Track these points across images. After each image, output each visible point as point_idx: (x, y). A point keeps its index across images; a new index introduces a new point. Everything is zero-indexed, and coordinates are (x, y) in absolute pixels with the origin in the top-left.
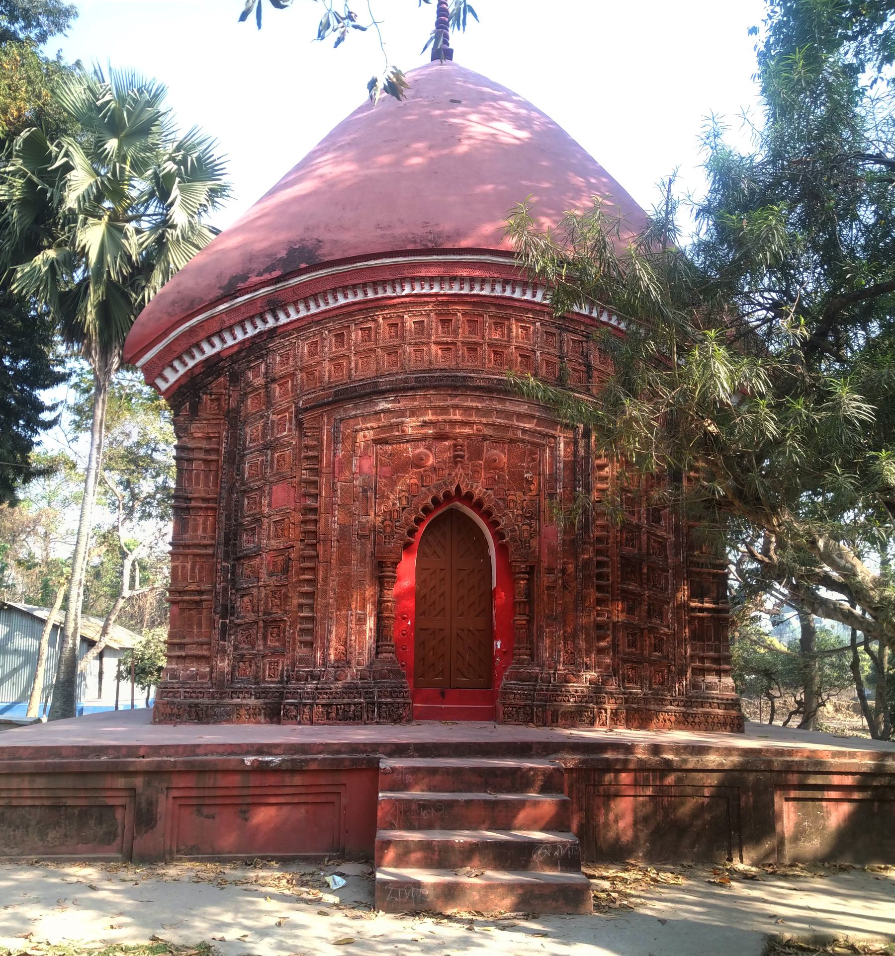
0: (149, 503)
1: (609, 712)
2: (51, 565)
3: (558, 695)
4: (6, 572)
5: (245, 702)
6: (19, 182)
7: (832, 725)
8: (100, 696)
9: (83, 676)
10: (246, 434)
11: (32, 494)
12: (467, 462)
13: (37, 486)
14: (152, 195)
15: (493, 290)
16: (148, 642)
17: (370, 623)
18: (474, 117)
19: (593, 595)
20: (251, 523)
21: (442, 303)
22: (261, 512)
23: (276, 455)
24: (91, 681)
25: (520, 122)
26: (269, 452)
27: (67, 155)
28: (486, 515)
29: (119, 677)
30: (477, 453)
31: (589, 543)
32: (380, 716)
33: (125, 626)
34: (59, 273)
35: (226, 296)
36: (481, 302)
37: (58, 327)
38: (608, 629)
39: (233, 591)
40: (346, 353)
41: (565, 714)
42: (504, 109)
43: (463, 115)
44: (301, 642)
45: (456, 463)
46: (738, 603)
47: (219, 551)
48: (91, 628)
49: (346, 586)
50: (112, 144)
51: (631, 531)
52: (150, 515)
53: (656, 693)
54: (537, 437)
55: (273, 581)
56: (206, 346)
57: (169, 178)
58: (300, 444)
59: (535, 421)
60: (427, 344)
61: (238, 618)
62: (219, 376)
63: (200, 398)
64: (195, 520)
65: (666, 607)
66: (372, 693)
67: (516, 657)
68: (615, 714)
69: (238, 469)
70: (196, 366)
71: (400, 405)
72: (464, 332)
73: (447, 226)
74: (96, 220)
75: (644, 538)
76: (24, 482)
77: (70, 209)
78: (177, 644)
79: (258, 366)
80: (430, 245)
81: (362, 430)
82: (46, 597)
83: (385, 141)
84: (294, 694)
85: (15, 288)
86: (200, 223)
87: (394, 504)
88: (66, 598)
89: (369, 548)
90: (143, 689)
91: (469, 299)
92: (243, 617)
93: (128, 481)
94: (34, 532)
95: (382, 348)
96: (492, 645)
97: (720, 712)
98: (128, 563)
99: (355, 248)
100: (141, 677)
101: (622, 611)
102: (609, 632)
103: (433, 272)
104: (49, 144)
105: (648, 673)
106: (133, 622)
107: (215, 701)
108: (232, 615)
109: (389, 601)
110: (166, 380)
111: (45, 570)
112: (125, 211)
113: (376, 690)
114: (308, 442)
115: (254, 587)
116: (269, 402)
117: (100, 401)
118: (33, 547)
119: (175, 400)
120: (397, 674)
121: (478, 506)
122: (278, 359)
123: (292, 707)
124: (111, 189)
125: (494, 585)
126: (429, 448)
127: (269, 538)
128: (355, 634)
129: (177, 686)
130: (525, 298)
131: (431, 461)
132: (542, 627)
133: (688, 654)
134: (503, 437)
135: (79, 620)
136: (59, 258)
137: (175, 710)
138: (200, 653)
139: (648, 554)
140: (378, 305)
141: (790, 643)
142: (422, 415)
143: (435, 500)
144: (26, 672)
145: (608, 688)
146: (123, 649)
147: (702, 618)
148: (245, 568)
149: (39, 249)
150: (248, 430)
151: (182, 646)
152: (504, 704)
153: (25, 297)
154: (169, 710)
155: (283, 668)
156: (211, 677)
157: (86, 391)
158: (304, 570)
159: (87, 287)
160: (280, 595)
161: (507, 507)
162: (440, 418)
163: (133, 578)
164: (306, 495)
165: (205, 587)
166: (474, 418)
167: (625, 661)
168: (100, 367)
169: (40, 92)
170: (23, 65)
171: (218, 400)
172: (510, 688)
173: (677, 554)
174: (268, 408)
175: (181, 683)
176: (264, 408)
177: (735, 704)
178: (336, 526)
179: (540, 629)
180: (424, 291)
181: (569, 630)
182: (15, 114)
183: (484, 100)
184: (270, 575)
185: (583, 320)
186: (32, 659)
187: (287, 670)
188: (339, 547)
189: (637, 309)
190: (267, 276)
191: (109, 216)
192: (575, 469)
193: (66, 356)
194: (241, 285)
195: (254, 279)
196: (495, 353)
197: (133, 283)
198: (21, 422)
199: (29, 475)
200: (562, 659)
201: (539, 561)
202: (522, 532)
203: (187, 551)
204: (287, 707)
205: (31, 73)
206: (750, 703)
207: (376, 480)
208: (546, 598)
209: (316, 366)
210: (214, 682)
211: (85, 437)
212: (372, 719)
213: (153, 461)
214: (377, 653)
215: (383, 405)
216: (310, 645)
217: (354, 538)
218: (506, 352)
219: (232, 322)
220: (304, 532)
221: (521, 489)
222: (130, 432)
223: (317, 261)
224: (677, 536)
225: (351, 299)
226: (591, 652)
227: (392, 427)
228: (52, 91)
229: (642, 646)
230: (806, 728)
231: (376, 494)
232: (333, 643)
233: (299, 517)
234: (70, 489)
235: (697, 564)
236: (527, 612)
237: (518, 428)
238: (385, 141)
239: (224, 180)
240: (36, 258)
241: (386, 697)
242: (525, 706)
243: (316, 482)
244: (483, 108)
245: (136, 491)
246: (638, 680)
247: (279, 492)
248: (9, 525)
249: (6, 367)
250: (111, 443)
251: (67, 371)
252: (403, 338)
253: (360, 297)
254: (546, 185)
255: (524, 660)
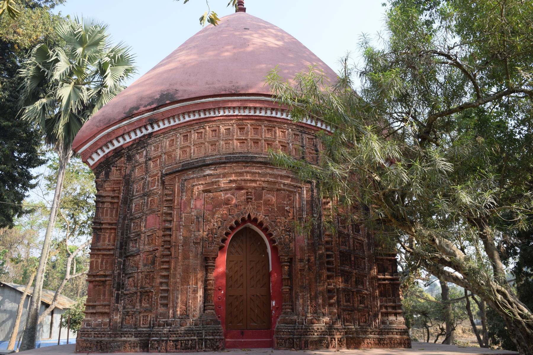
0: (84, 226)
1: (336, 340)
2: (30, 261)
3: (308, 332)
4: (4, 265)
5: (128, 339)
6: (32, 68)
7: (461, 341)
8: (50, 337)
9: (41, 324)
10: (134, 188)
11: (21, 222)
12: (254, 201)
13: (25, 219)
14: (97, 72)
15: (266, 113)
16: (79, 305)
17: (200, 293)
18: (255, 35)
19: (325, 273)
20: (136, 236)
21: (240, 119)
22: (140, 231)
23: (150, 199)
24: (46, 328)
25: (276, 37)
26: (146, 198)
27: (57, 55)
28: (265, 230)
29: (61, 325)
30: (259, 197)
31: (322, 245)
32: (206, 347)
33: (68, 296)
34: (47, 110)
35: (127, 117)
36: (260, 119)
37: (43, 137)
38: (334, 292)
39: (124, 275)
40: (189, 145)
41: (312, 342)
42: (270, 32)
43: (250, 34)
44: (161, 304)
45: (248, 202)
46: (406, 275)
47: (117, 252)
48: (48, 297)
49: (186, 271)
50: (80, 50)
51: (344, 238)
52: (84, 233)
53: (362, 327)
54: (291, 188)
55: (146, 269)
56: (115, 142)
57: (106, 64)
58: (163, 193)
59: (290, 179)
60: (232, 140)
61: (126, 290)
62: (121, 158)
63: (110, 169)
64: (104, 235)
65: (365, 278)
66: (201, 333)
67: (284, 310)
68: (340, 341)
69: (129, 207)
70: (109, 152)
71: (218, 172)
72: (251, 134)
73: (242, 83)
74: (68, 85)
75: (351, 241)
76: (18, 217)
77: (56, 80)
78: (91, 306)
79: (142, 152)
80: (233, 92)
81: (196, 185)
82: (25, 279)
83: (212, 45)
84: (156, 335)
85: (24, 118)
86: (119, 85)
87: (214, 225)
88: (35, 280)
89: (200, 250)
90: (74, 332)
91: (254, 118)
92: (128, 290)
93: (73, 214)
94: (21, 243)
95: (208, 142)
96: (270, 304)
97: (398, 337)
98: (70, 260)
99: (195, 93)
100: (73, 326)
101: (342, 282)
102: (335, 294)
103: (235, 105)
104: (49, 50)
105: (357, 316)
106: (72, 293)
107: (111, 339)
108: (123, 288)
109: (211, 280)
110: (93, 160)
111: (26, 264)
112: (83, 80)
113: (204, 332)
114: (167, 192)
115: (135, 272)
116: (147, 171)
117: (62, 173)
118: (21, 251)
119: (97, 170)
120: (216, 322)
121: (260, 225)
122: (153, 148)
123: (156, 342)
124: (76, 70)
125: (271, 269)
126: (233, 194)
127: (144, 245)
128: (192, 300)
129: (90, 330)
130: (283, 117)
131: (234, 201)
132: (298, 292)
133: (379, 305)
134: (273, 188)
135: (41, 292)
136: (48, 103)
137: (89, 345)
138: (104, 311)
139: (354, 250)
140: (206, 121)
141: (436, 296)
142: (229, 177)
143: (237, 223)
144: (9, 323)
145: (336, 326)
146: (65, 309)
147: (385, 284)
148: (131, 262)
149: (38, 98)
150: (135, 186)
151: (94, 307)
152: (277, 338)
153: (28, 121)
154: (85, 345)
155: (151, 319)
156: (110, 325)
157: (55, 169)
158: (163, 262)
159: (60, 116)
160: (150, 277)
161: (276, 225)
162: (239, 178)
163: (72, 268)
164: (165, 221)
165: (108, 273)
166: (257, 178)
167: (344, 310)
168: (63, 156)
169: (48, 29)
170: (42, 17)
171: (120, 170)
172: (281, 329)
173: (369, 249)
174: (146, 174)
175: (93, 328)
176: (144, 174)
177: (405, 332)
178: (182, 237)
179: (296, 293)
180: (230, 114)
181: (313, 294)
182: (35, 38)
183: (260, 28)
184: (145, 265)
185: (313, 128)
186: (14, 315)
187: (153, 321)
188: (183, 250)
189: (334, 119)
190: (149, 107)
191: (75, 83)
192: (312, 204)
193: (46, 151)
194: (135, 112)
195: (142, 109)
196: (268, 144)
197: (84, 114)
198: (20, 185)
199: (20, 212)
200: (309, 311)
201: (295, 255)
202: (285, 239)
203: (99, 253)
204: (153, 342)
205: (45, 21)
206: (418, 331)
207: (204, 212)
208: (299, 276)
209: (173, 151)
210: (111, 327)
211: (52, 192)
212: (201, 349)
213: (87, 203)
214: (204, 310)
215: (208, 172)
216: (166, 305)
217: (192, 244)
218: (274, 144)
219: (130, 130)
220: (164, 241)
221: (283, 215)
222: (76, 188)
223: (175, 100)
224: (369, 239)
225: (192, 118)
226: (325, 306)
227: (213, 183)
228: (54, 28)
229: (353, 301)
230: (448, 343)
231: (204, 220)
232: (179, 304)
233: (162, 233)
234: (43, 219)
235: (381, 254)
236: (289, 284)
237: (281, 183)
238: (212, 45)
239: (133, 65)
240: (36, 103)
241: (210, 336)
242: (289, 339)
243: (171, 214)
244: (260, 32)
245: (77, 219)
246: (352, 320)
247: (151, 219)
248: (9, 239)
249: (15, 157)
250: (66, 194)
251: (47, 159)
252: (219, 137)
253: (197, 117)
254: (292, 65)
255: (289, 312)
